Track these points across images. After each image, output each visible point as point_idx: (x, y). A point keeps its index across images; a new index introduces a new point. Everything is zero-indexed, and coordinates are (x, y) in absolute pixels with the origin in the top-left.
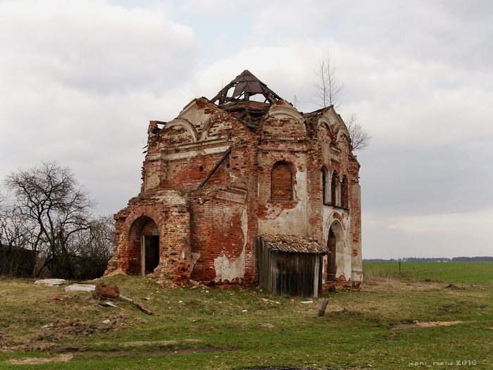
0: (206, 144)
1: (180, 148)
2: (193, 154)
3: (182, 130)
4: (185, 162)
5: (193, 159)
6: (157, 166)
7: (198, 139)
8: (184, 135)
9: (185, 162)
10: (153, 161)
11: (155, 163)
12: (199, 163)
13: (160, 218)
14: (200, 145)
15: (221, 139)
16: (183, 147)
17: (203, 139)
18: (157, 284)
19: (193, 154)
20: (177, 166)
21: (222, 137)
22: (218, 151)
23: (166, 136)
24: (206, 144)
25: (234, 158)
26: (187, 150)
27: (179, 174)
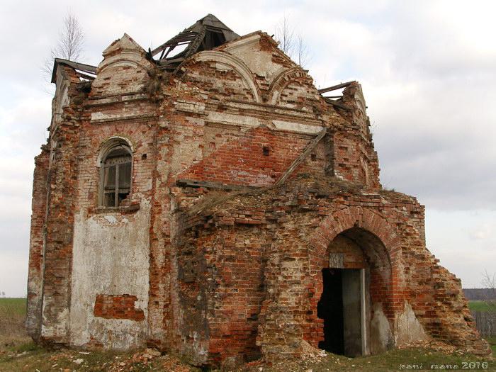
0: (281, 112)
1: (232, 104)
2: (251, 122)
3: (233, 75)
4: (235, 133)
5: (253, 131)
6: (195, 125)
7: (265, 100)
8: (235, 84)
9: (235, 133)
10: (190, 114)
11: (192, 120)
12: (264, 141)
13: (394, 235)
14: (268, 111)
15: (302, 112)
16: (237, 105)
17: (273, 102)
18: (40, 326)
19: (251, 122)
20: (219, 136)
21: (304, 109)
22: (296, 129)
23: (196, 75)
24: (281, 112)
25: (341, 148)
26: (242, 112)
27: (222, 151)
